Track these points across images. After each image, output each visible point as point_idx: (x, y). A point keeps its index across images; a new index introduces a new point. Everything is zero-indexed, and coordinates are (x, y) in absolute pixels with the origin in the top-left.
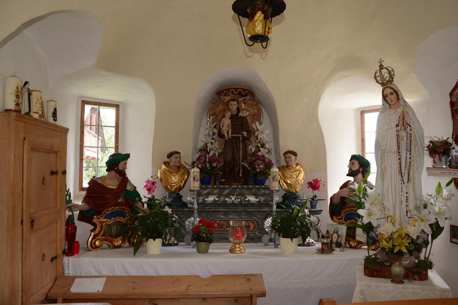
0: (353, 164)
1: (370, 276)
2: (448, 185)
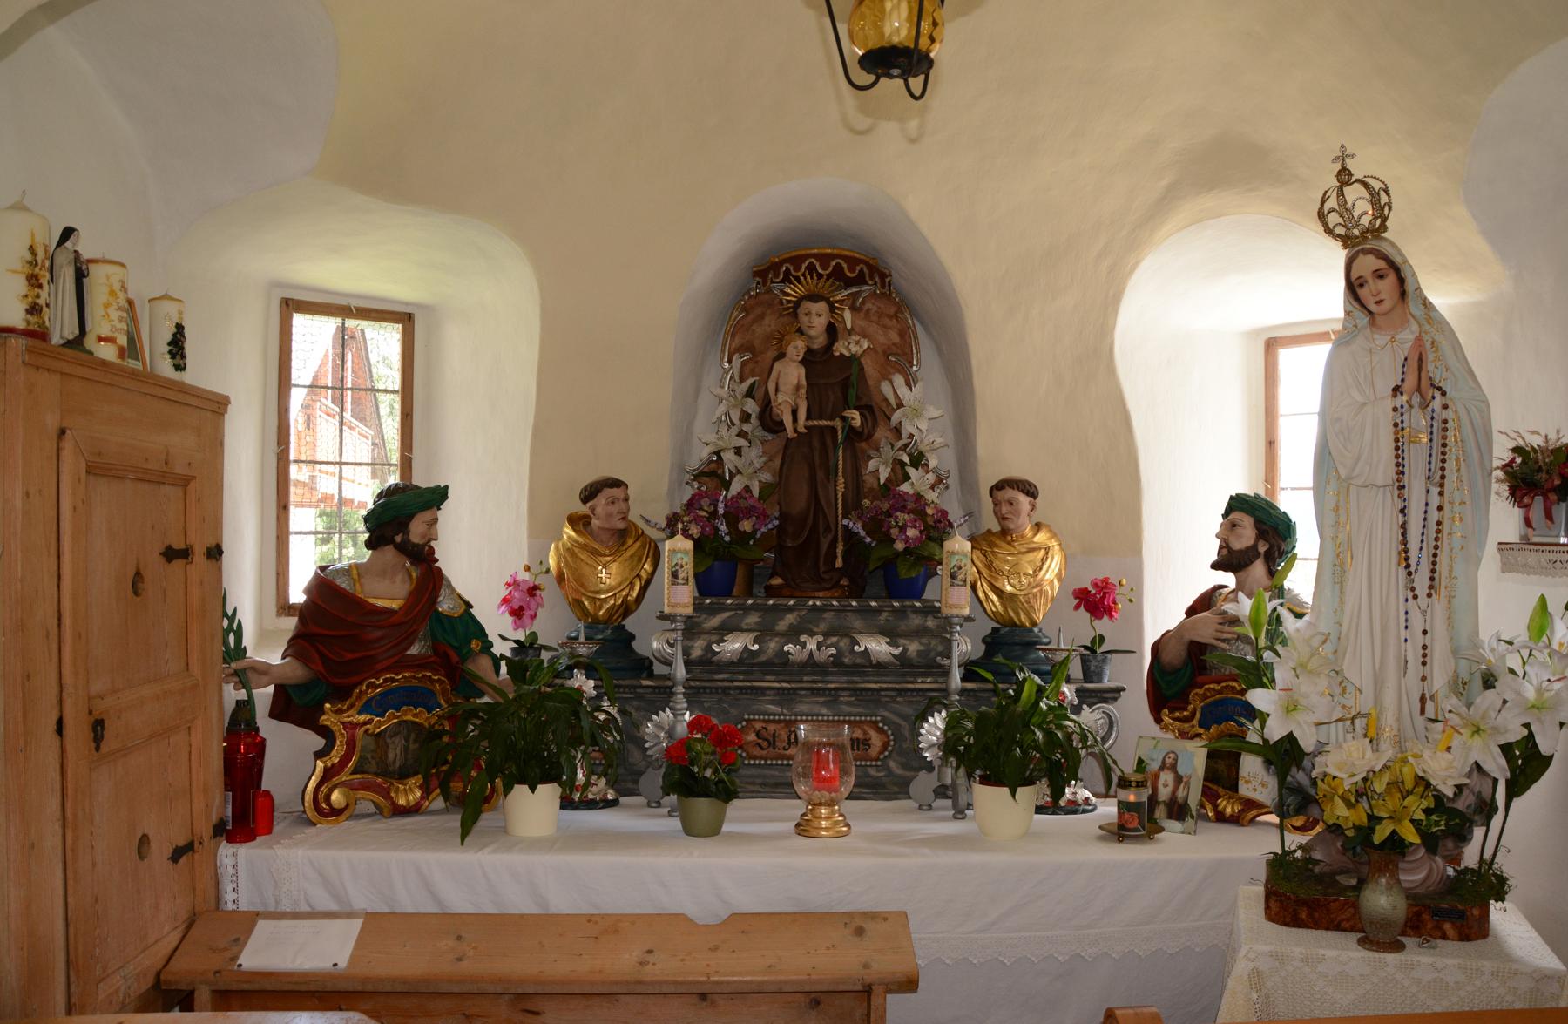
0: (1234, 525)
1: (1286, 924)
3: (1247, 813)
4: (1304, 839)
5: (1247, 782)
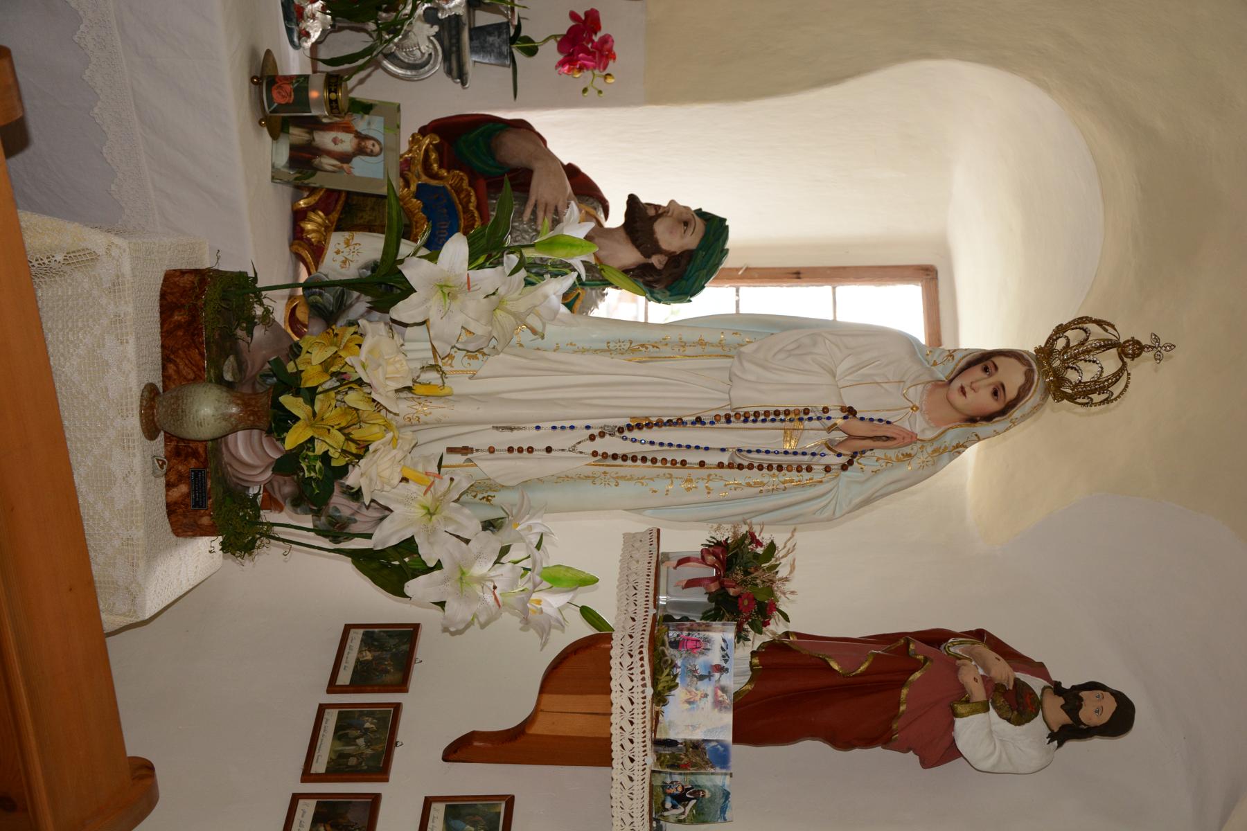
0: (686, 224)
1: (163, 296)
2: (586, 612)
3: (306, 248)
4: (280, 315)
5: (347, 244)
